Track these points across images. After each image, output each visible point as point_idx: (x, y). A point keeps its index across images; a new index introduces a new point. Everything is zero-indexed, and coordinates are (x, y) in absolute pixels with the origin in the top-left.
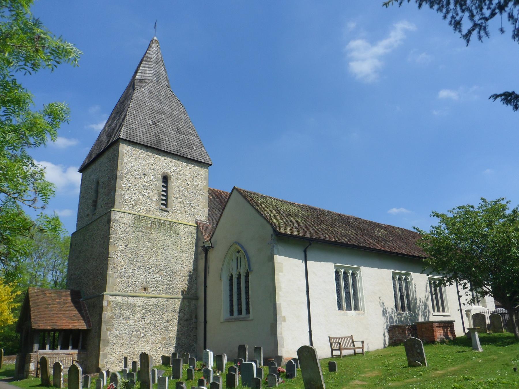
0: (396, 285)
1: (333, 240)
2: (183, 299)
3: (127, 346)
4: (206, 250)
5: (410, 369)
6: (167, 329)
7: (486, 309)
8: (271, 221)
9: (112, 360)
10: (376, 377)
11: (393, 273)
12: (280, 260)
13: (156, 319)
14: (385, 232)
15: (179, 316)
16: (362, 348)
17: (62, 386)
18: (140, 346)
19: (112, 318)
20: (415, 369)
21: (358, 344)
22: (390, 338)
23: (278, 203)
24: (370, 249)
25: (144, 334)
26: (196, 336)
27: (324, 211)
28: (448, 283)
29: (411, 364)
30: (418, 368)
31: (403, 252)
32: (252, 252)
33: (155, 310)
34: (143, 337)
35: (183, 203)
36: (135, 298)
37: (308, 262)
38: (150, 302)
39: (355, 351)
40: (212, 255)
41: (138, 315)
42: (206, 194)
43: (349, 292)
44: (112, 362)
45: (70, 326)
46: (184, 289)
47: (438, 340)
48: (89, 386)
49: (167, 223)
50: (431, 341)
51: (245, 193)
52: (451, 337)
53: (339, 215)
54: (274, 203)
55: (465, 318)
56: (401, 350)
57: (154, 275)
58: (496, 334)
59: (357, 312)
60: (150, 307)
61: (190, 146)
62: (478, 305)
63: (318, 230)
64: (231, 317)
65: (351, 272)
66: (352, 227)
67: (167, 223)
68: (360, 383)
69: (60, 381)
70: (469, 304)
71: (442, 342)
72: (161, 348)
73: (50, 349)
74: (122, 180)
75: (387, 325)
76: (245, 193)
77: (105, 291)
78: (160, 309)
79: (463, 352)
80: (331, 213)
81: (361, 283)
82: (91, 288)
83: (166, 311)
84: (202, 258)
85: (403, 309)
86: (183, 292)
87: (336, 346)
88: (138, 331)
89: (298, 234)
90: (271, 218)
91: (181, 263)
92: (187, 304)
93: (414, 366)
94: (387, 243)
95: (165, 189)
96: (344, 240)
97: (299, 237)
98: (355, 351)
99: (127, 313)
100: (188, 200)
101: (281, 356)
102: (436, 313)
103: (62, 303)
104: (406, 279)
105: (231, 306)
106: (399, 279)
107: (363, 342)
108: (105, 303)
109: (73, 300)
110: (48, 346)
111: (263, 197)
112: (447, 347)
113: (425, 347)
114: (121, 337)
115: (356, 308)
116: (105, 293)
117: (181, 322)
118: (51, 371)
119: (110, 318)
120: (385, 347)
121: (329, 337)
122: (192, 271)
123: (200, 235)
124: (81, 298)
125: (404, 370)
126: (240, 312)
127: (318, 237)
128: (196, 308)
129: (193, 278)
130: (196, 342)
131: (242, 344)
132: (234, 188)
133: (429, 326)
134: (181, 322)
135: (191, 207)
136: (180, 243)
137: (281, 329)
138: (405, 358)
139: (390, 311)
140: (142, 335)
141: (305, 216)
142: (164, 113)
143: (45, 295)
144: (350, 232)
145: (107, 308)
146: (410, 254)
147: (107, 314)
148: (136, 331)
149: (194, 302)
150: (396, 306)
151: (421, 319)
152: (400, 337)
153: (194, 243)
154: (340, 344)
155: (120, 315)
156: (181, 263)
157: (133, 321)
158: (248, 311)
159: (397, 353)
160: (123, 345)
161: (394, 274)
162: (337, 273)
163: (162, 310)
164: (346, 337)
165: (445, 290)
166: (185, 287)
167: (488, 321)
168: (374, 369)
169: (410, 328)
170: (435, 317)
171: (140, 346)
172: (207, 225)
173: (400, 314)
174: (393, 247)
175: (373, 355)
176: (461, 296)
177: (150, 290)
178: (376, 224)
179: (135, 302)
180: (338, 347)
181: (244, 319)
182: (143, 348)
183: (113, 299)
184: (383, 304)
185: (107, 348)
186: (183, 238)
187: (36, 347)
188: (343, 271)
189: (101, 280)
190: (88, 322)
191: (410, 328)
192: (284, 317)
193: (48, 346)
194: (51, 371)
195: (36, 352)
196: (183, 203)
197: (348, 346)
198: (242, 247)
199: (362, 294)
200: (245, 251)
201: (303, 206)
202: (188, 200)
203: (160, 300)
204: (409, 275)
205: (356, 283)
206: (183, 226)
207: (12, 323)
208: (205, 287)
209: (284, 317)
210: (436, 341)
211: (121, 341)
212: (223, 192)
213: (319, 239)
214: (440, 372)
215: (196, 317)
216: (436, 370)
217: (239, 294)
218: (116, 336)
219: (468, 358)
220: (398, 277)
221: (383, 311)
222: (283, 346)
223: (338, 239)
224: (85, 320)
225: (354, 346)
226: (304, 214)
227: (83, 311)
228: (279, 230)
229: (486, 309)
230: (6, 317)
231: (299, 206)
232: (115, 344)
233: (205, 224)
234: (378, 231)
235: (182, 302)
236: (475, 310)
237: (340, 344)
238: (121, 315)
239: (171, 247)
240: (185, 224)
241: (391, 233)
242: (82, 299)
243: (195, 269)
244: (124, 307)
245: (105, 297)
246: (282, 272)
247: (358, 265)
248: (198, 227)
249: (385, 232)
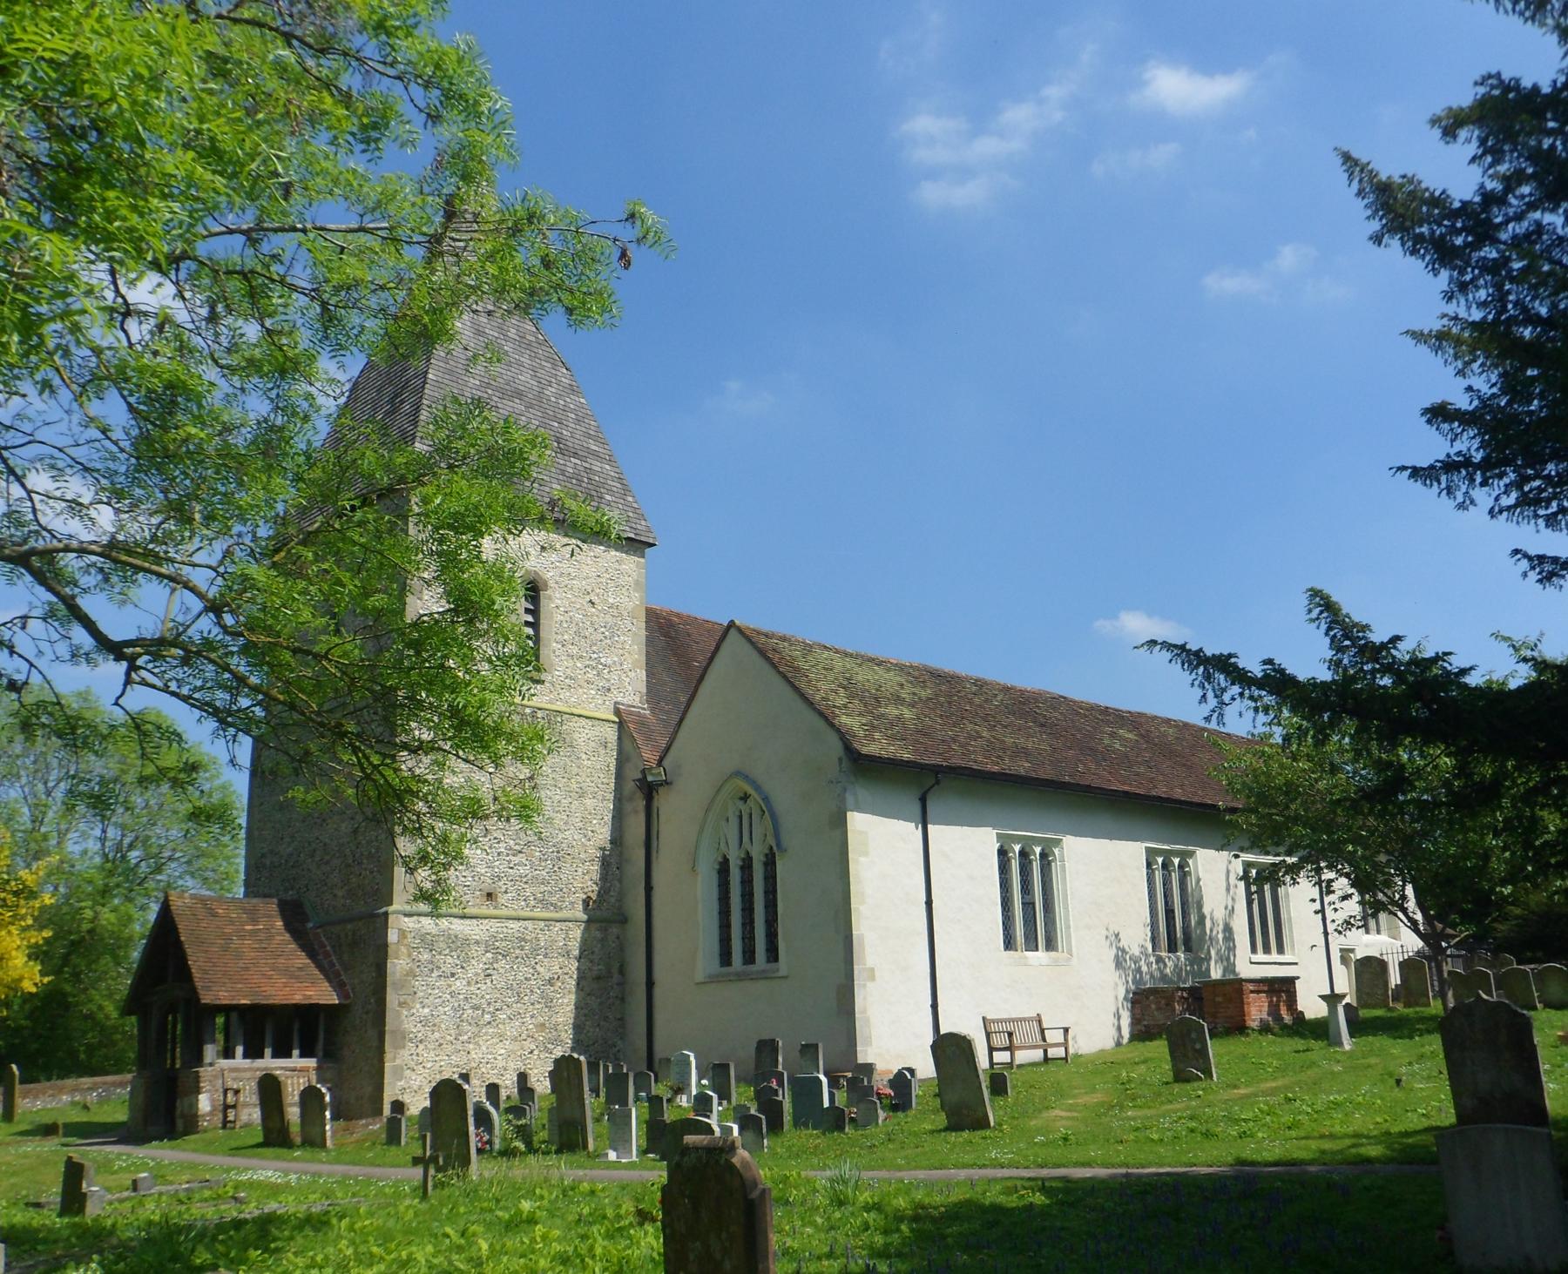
0: (1155, 895)
1: (996, 769)
2: (588, 922)
3: (450, 1048)
4: (649, 790)
5: (1177, 1088)
6: (549, 1003)
7: (1399, 943)
8: (836, 722)
9: (415, 1084)
10: (1102, 1104)
11: (1148, 850)
12: (859, 823)
13: (520, 977)
14: (1130, 736)
15: (578, 969)
16: (1065, 1045)
17: (329, 1143)
18: (484, 1048)
19: (411, 974)
20: (1188, 1087)
21: (1054, 1037)
22: (1135, 1021)
23: (849, 663)
24: (1088, 790)
25: (493, 1014)
26: (621, 1019)
27: (967, 679)
28: (1288, 878)
29: (1180, 1077)
30: (1196, 1084)
31: (1178, 794)
32: (784, 798)
33: (518, 951)
34: (489, 1023)
35: (581, 657)
36: (468, 922)
37: (930, 827)
38: (505, 930)
39: (1045, 1052)
40: (666, 803)
41: (476, 967)
42: (640, 628)
43: (1034, 904)
44: (415, 1088)
45: (297, 997)
46: (590, 894)
47: (1255, 1024)
48: (403, 1143)
49: (540, 714)
50: (1238, 1027)
51: (763, 639)
52: (1287, 1018)
53: (1006, 689)
54: (838, 664)
55: (1339, 969)
56: (1159, 1048)
57: (511, 857)
58: (1409, 1011)
59: (1053, 954)
60: (504, 944)
61: (593, 495)
62: (1378, 932)
63: (954, 740)
64: (725, 970)
65: (1038, 850)
66: (1042, 725)
67: (540, 714)
68: (1064, 1114)
69: (324, 1132)
70: (1340, 933)
71: (1265, 1029)
72: (536, 1052)
73: (246, 1056)
74: (420, 599)
75: (1127, 991)
76: (763, 639)
77: (391, 904)
78: (525, 949)
79: (1308, 1050)
80: (986, 683)
81: (1064, 879)
82: (340, 893)
83: (546, 956)
84: (636, 812)
85: (1172, 948)
86: (586, 902)
87: (998, 1041)
88: (477, 1009)
89: (906, 756)
90: (837, 711)
91: (580, 824)
92: (598, 934)
93: (1188, 1081)
94: (1135, 769)
95: (530, 619)
96: (1023, 767)
97: (908, 764)
98: (1045, 1052)
99: (450, 960)
100: (594, 648)
101: (871, 1065)
102: (1260, 956)
103: (262, 936)
104: (1181, 867)
105: (725, 941)
106: (1165, 866)
107: (1066, 1030)
108: (392, 936)
109: (288, 927)
110: (239, 1050)
111: (808, 648)
112: (1274, 1042)
113: (1217, 1042)
114: (434, 1025)
115: (1051, 945)
116: (391, 909)
117: (583, 983)
118: (293, 1113)
119: (407, 975)
120: (1118, 1044)
121: (984, 1018)
122: (608, 846)
123: (628, 746)
124: (308, 921)
125: (1164, 1089)
126: (749, 957)
127: (957, 761)
128: (621, 948)
129: (612, 863)
130: (622, 1037)
131: (767, 1037)
132: (732, 624)
133: (1234, 988)
134: (583, 983)
135: (600, 668)
136: (575, 770)
137: (865, 998)
138: (1168, 1067)
139: (1136, 951)
140: (487, 1017)
141: (920, 698)
142: (519, 394)
143: (215, 915)
144: (1038, 742)
145: (399, 949)
146: (1196, 799)
147: (398, 965)
148: (472, 1008)
149: (615, 930)
150: (1154, 939)
151: (1216, 973)
152: (1160, 1018)
153: (613, 768)
154: (1010, 1034)
155: (430, 966)
156: (580, 824)
157: (464, 983)
158: (773, 953)
159: (1150, 1055)
160: (440, 1045)
161: (1151, 853)
162: (1002, 853)
163: (535, 951)
164: (1024, 1020)
165: (1287, 894)
166: (593, 889)
167: (1395, 978)
168: (1094, 1090)
169: (1185, 995)
170: (1250, 965)
171: (484, 1048)
172: (644, 716)
173: (1159, 960)
174: (1151, 780)
175: (1092, 1062)
176: (1316, 912)
177: (502, 899)
178: (1106, 711)
179: (467, 931)
180: (1005, 1042)
181: (763, 976)
182: (491, 1053)
183: (411, 925)
184: (1117, 935)
185: (402, 1052)
186: (584, 756)
187: (210, 1051)
188: (1017, 848)
189: (372, 872)
190: (339, 986)
191: (1185, 995)
192: (872, 970)
193: (239, 1050)
194: (293, 1113)
195: (211, 1065)
196: (581, 657)
197: (1030, 1042)
198: (758, 788)
199: (1066, 908)
200: (766, 799)
201: (911, 667)
202: (594, 648)
203: (529, 924)
204: (1191, 854)
205: (1051, 879)
206: (583, 722)
207: (34, 990)
208: (649, 889)
209: (872, 970)
210: (1247, 1028)
211: (437, 1035)
212: (678, 615)
213: (960, 768)
214: (1242, 1091)
215: (622, 971)
216: (1235, 1087)
217: (748, 909)
218: (424, 1022)
219: (1313, 1064)
220: (1160, 860)
221: (1117, 957)
222: (868, 1042)
223: (1008, 765)
224: (330, 981)
225: (1044, 1039)
226: (914, 694)
227: (320, 957)
228: (858, 747)
229: (1399, 943)
230: (18, 972)
231: (901, 668)
232: (421, 1041)
233: (639, 715)
234: (1113, 735)
235: (586, 930)
236: (1366, 946)
237: (1010, 1034)
238: (433, 966)
239: (553, 782)
240: (587, 718)
241: (1146, 737)
242: (310, 925)
243: (617, 840)
244: (441, 945)
245: (391, 918)
246: (866, 854)
247: (1056, 833)
248: (621, 725)
249: (1130, 736)
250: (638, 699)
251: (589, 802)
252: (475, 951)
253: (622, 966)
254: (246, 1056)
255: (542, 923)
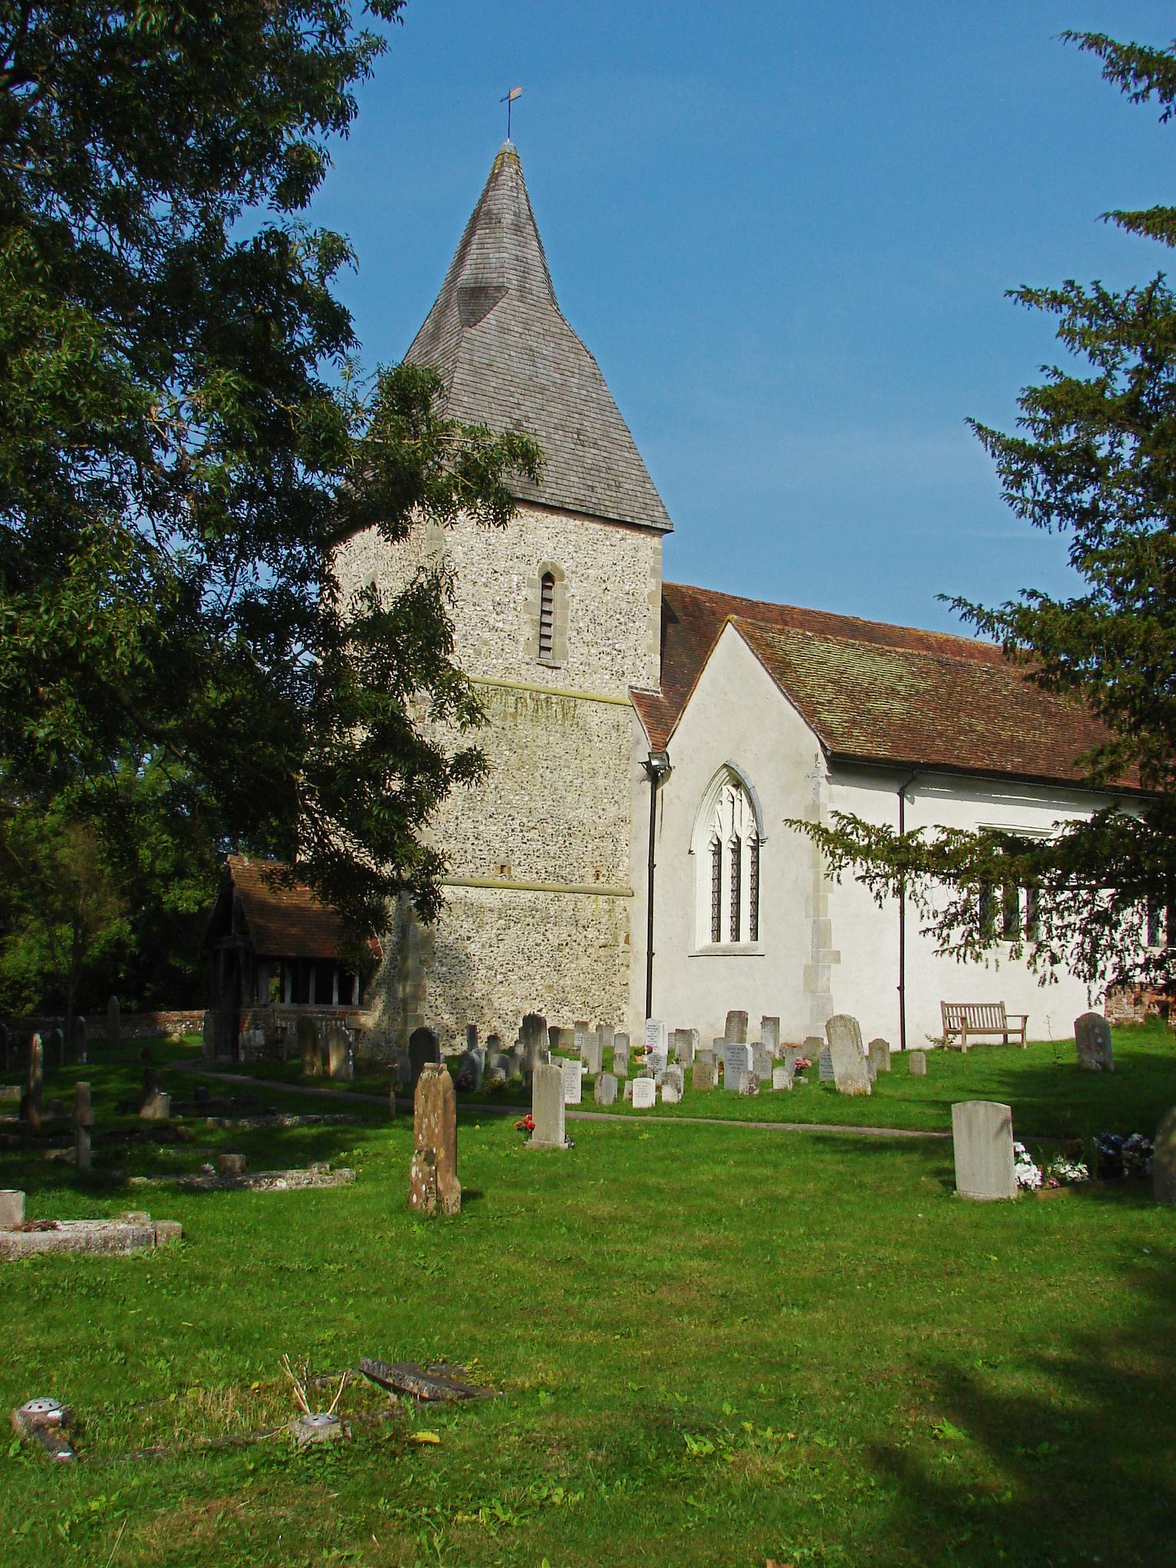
16: (1022, 1032)
49: (554, 699)
63: (941, 735)
88: (491, 969)
89: (883, 753)
90: (819, 708)
96: (1011, 763)
107: (1025, 1018)
136: (587, 752)
140: (500, 977)
177: (516, 872)
186: (596, 739)
202: (609, 635)
206: (594, 706)
211: (454, 991)
250: (651, 682)
251: (601, 782)
252: (489, 917)
253: (627, 937)
254: (293, 1000)
255: (552, 895)
